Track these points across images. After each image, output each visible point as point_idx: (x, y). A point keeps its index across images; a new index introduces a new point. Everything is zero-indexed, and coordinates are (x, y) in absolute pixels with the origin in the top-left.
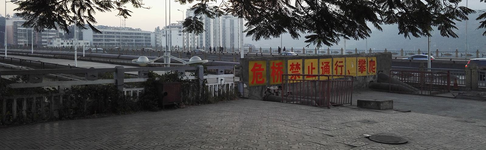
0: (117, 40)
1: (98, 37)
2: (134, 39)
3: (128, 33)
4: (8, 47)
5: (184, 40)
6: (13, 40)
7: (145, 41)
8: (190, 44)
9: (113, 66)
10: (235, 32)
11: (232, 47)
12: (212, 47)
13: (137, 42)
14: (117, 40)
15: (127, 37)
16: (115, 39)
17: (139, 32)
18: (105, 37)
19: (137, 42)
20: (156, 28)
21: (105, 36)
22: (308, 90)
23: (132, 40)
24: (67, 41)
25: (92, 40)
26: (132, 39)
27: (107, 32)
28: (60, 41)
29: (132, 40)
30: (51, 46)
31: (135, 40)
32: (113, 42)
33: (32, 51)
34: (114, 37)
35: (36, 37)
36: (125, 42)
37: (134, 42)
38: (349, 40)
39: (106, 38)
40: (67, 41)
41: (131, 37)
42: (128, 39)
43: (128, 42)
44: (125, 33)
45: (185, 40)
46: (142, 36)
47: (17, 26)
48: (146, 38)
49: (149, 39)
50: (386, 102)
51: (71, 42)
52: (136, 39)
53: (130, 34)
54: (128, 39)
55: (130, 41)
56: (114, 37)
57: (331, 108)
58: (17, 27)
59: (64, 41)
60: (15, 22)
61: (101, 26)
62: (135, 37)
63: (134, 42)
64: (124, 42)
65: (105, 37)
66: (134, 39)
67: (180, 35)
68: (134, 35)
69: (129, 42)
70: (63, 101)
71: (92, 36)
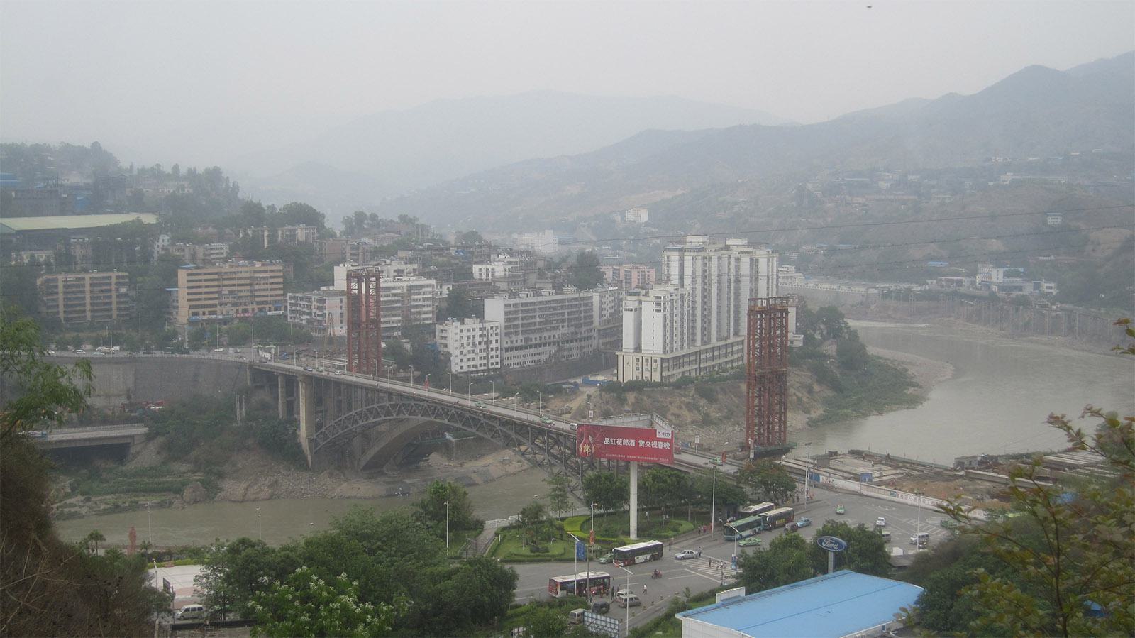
0: (540, 316)
2: (566, 311)
7: (522, 326)
8: (762, 284)
9: (1001, 476)
14: (540, 316)
15: (554, 308)
18: (522, 320)
21: (522, 310)
23: (563, 314)
26: (563, 311)
29: (563, 314)
30: (445, 349)
31: (568, 312)
32: (533, 321)
34: (535, 310)
35: (64, 312)
37: (566, 316)
44: (553, 301)
48: (586, 305)
50: (360, 390)
52: (569, 310)
56: (535, 310)
66: (566, 311)
68: (567, 304)
70: (220, 347)
71: (503, 306)
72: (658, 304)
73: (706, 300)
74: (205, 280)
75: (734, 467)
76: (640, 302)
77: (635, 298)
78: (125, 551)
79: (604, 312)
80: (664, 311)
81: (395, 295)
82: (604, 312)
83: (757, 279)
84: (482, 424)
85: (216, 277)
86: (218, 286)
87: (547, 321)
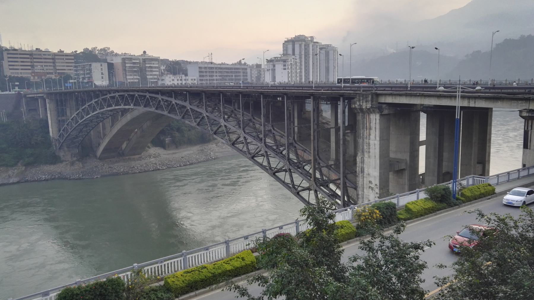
1: (203, 73)
2: (234, 75)
3: (229, 68)
4: (439, 85)
5: (288, 75)
6: (122, 78)
10: (330, 65)
11: (327, 80)
12: (311, 80)
13: (236, 78)
14: (220, 76)
15: (227, 72)
16: (215, 74)
17: (212, 66)
18: (209, 73)
19: (236, 78)
20: (76, 51)
21: (209, 71)
22: (117, 174)
24: (177, 78)
25: (198, 76)
27: (211, 67)
28: (172, 77)
29: (232, 76)
31: (235, 75)
33: (242, 85)
36: (226, 78)
37: (234, 77)
38: (267, 59)
39: (209, 74)
40: (177, 78)
41: (231, 72)
42: (229, 74)
43: (229, 78)
45: (290, 75)
46: (240, 71)
47: (125, 62)
49: (246, 74)
51: (181, 78)
53: (230, 70)
54: (229, 74)
55: (231, 76)
57: (181, 212)
58: (125, 64)
59: (175, 78)
60: (123, 59)
61: (182, 60)
62: (235, 72)
63: (234, 77)
64: (225, 78)
65: (209, 73)
66: (234, 75)
67: (285, 69)
68: (234, 70)
69: (230, 78)
72: (285, 65)
73: (307, 68)
74: (21, 58)
75: (124, 148)
76: (274, 66)
77: (272, 63)
78: (9, 168)
79: (253, 75)
80: (288, 69)
81: (134, 63)
82: (253, 79)
83: (328, 62)
84: (203, 118)
85: (28, 56)
86: (31, 62)
87: (223, 79)
